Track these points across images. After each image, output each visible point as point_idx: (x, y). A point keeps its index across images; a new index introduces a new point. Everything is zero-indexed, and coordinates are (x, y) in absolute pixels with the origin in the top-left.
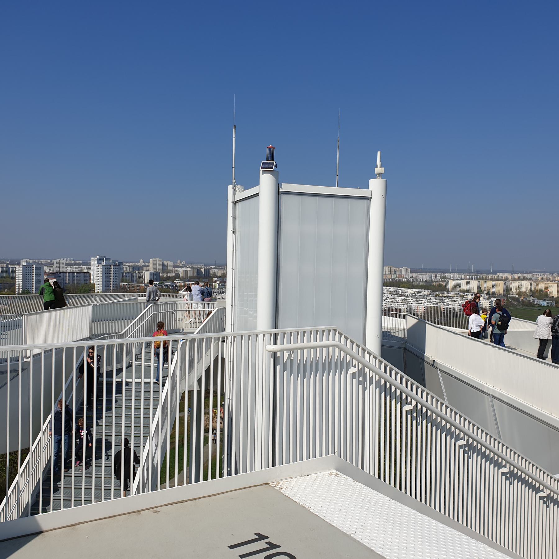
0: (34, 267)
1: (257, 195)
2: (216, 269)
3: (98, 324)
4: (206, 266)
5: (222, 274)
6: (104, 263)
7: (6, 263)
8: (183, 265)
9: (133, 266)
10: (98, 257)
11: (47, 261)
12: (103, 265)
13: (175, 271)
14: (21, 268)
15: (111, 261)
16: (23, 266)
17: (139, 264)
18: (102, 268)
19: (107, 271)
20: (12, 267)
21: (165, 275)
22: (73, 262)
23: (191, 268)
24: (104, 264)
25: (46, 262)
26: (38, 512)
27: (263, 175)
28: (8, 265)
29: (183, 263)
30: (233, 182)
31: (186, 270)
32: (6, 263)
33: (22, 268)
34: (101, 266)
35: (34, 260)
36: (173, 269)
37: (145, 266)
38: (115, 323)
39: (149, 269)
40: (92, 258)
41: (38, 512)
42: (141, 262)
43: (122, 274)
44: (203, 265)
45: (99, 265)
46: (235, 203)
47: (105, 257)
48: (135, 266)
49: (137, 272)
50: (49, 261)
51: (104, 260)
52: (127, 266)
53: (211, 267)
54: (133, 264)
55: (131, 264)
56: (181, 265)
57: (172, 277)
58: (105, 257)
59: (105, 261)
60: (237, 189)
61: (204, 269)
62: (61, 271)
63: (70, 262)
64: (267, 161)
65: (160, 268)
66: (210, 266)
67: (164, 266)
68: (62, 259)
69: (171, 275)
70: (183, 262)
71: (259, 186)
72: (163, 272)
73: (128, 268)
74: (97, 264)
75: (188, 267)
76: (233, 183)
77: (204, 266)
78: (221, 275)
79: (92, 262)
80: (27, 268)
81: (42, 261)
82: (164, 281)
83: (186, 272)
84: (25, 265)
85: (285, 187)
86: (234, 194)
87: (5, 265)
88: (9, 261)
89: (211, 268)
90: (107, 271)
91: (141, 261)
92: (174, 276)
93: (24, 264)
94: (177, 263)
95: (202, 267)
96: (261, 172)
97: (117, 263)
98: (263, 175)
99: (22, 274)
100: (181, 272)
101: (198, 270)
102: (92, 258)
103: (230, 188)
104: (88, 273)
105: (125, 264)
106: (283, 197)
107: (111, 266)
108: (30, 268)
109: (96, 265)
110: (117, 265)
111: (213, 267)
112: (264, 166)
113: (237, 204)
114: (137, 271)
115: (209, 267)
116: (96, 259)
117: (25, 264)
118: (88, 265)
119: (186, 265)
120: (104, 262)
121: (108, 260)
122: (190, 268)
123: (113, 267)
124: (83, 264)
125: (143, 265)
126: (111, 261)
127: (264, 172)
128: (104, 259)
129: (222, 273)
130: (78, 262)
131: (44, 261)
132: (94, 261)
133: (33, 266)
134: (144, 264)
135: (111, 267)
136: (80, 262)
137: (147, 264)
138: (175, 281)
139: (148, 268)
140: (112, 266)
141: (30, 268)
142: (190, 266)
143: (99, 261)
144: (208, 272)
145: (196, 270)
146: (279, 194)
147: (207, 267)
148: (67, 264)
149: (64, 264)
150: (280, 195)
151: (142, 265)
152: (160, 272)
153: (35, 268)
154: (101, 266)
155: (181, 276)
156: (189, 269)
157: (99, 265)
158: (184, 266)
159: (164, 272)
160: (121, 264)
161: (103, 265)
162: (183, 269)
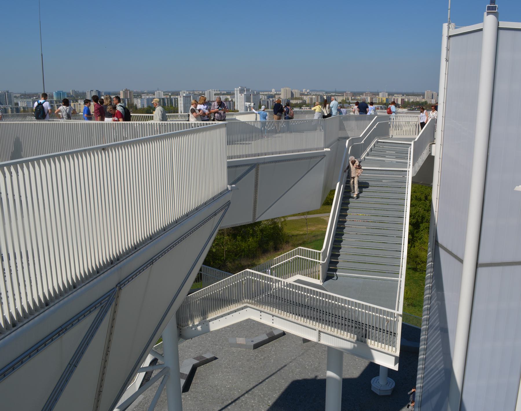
0: (192, 97)
1: (481, 30)
2: (337, 96)
3: (281, 136)
4: (328, 93)
5: (341, 100)
6: (246, 93)
7: (168, 95)
8: (307, 93)
9: (267, 95)
10: (240, 87)
11: (199, 92)
12: (244, 95)
13: (301, 98)
14: (182, 98)
15: (250, 91)
16: (183, 96)
17: (272, 93)
18: (244, 96)
19: (248, 99)
20: (174, 98)
21: (293, 102)
22: (219, 92)
23: (316, 95)
24: (245, 93)
25: (199, 93)
26: (325, 230)
27: (487, 15)
28: (170, 96)
29: (307, 91)
30: (448, 20)
31: (311, 97)
32: (168, 95)
33: (182, 98)
34: (243, 95)
35: (190, 92)
36: (300, 96)
37: (276, 94)
38: (267, 141)
39: (280, 97)
40: (236, 89)
41: (325, 230)
42: (273, 91)
43: (260, 102)
44: (325, 93)
45: (241, 95)
46: (449, 37)
47: (245, 87)
48: (268, 95)
49: (271, 99)
50: (201, 92)
51: (244, 90)
52: (262, 95)
53: (332, 95)
54: (267, 93)
55: (265, 93)
56: (306, 93)
57: (300, 103)
58: (245, 87)
59: (245, 91)
60: (450, 26)
61: (327, 96)
62: (211, 100)
63: (217, 92)
64: (490, 4)
65: (289, 96)
66: (330, 94)
67: (292, 94)
68: (211, 90)
69: (299, 102)
70: (308, 91)
71: (483, 23)
72: (292, 99)
73: (264, 96)
74: (240, 93)
75: (312, 94)
76: (448, 22)
77: (326, 93)
78: (341, 101)
79: (236, 92)
80: (187, 98)
81: (195, 92)
82: (293, 107)
83: (311, 99)
84: (185, 95)
85: (502, 24)
86: (448, 30)
87: (168, 97)
88: (170, 93)
89: (332, 96)
90: (248, 99)
91: (273, 90)
92: (301, 103)
93: (184, 95)
94: (302, 91)
95: (324, 94)
96: (485, 13)
97: (255, 92)
98: (487, 15)
99: (183, 103)
100: (307, 99)
101: (321, 97)
102: (236, 89)
103: (445, 25)
104: (232, 101)
105: (261, 93)
106: (501, 32)
107: (251, 95)
108: (188, 98)
109: (239, 95)
110: (255, 94)
111: (333, 94)
112: (489, 8)
113: (451, 39)
114: (271, 99)
115: (330, 94)
116: (238, 89)
117: (184, 95)
118: (232, 94)
119: (310, 93)
120: (244, 91)
121: (248, 90)
122: (313, 95)
123: (253, 96)
124: (228, 94)
125: (275, 94)
126: (250, 91)
127: (488, 14)
128: (245, 89)
129: (342, 99)
130: (223, 92)
131: (197, 92)
132: (237, 91)
133: (191, 96)
134: (275, 93)
135: (251, 96)
136: (225, 92)
137: (278, 93)
138: (302, 107)
139: (279, 96)
140: (252, 95)
141: (188, 98)
142: (314, 94)
143: (242, 91)
144: (330, 99)
145: (319, 97)
146: (499, 29)
147: (329, 94)
148: (215, 95)
149: (213, 95)
150: (499, 31)
151: (274, 94)
152: (290, 100)
153: (193, 98)
154: (243, 95)
155: (307, 103)
156: (314, 97)
157: (241, 95)
158: (309, 94)
159: (293, 100)
160: (258, 94)
161: (244, 95)
162: (308, 96)
